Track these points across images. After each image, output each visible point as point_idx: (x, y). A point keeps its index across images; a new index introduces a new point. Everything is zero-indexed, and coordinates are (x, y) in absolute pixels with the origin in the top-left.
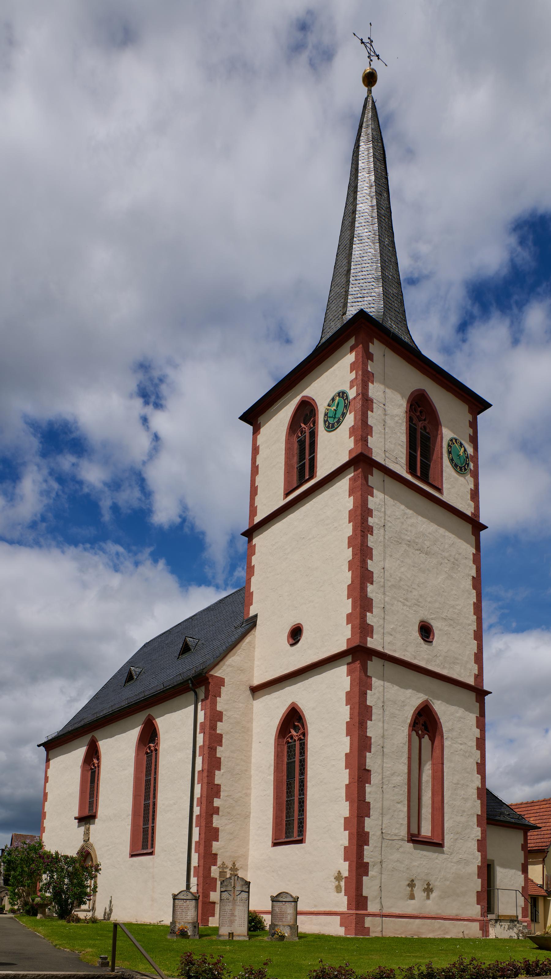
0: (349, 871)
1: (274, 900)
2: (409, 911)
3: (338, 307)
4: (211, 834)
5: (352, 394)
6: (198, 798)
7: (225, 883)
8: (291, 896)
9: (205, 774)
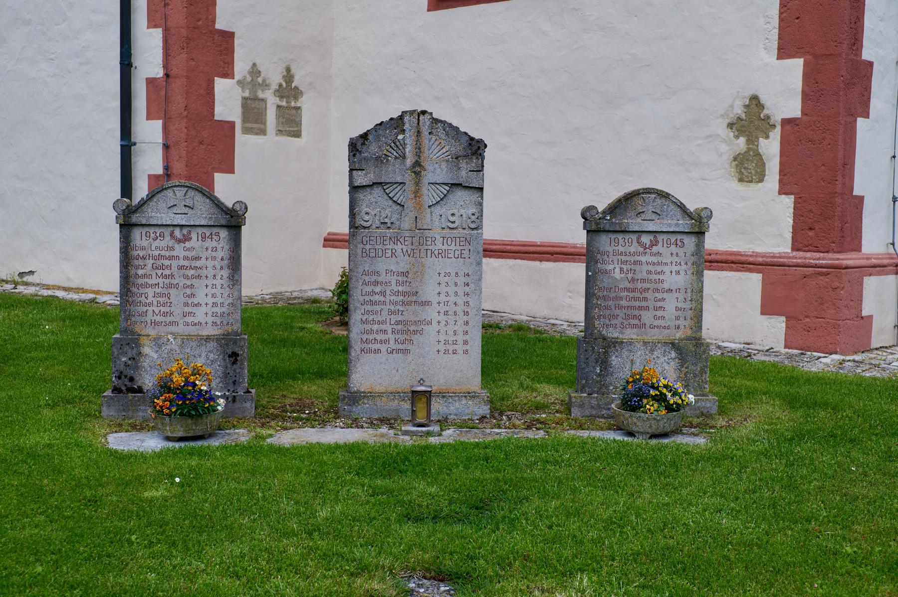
0: (806, 96)
7: (373, 148)
8: (682, 207)
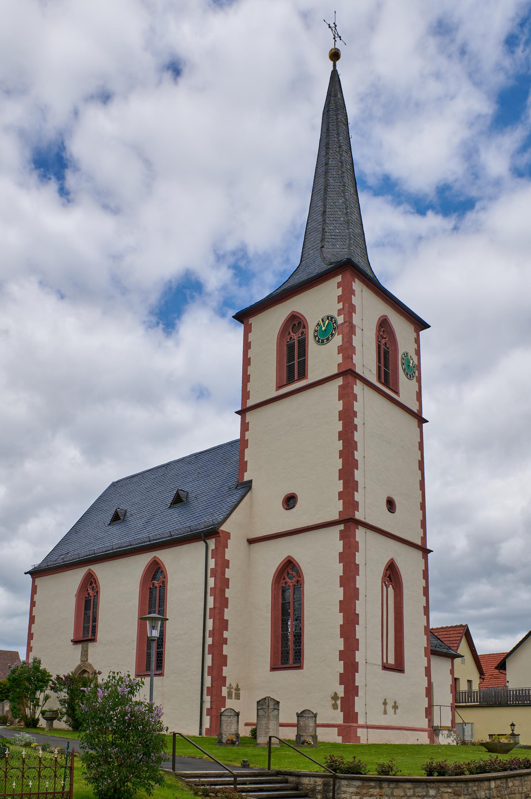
1: (299, 716)
2: (383, 723)
3: (316, 240)
4: (221, 661)
5: (340, 320)
6: (210, 631)
7: (261, 703)
9: (217, 611)
